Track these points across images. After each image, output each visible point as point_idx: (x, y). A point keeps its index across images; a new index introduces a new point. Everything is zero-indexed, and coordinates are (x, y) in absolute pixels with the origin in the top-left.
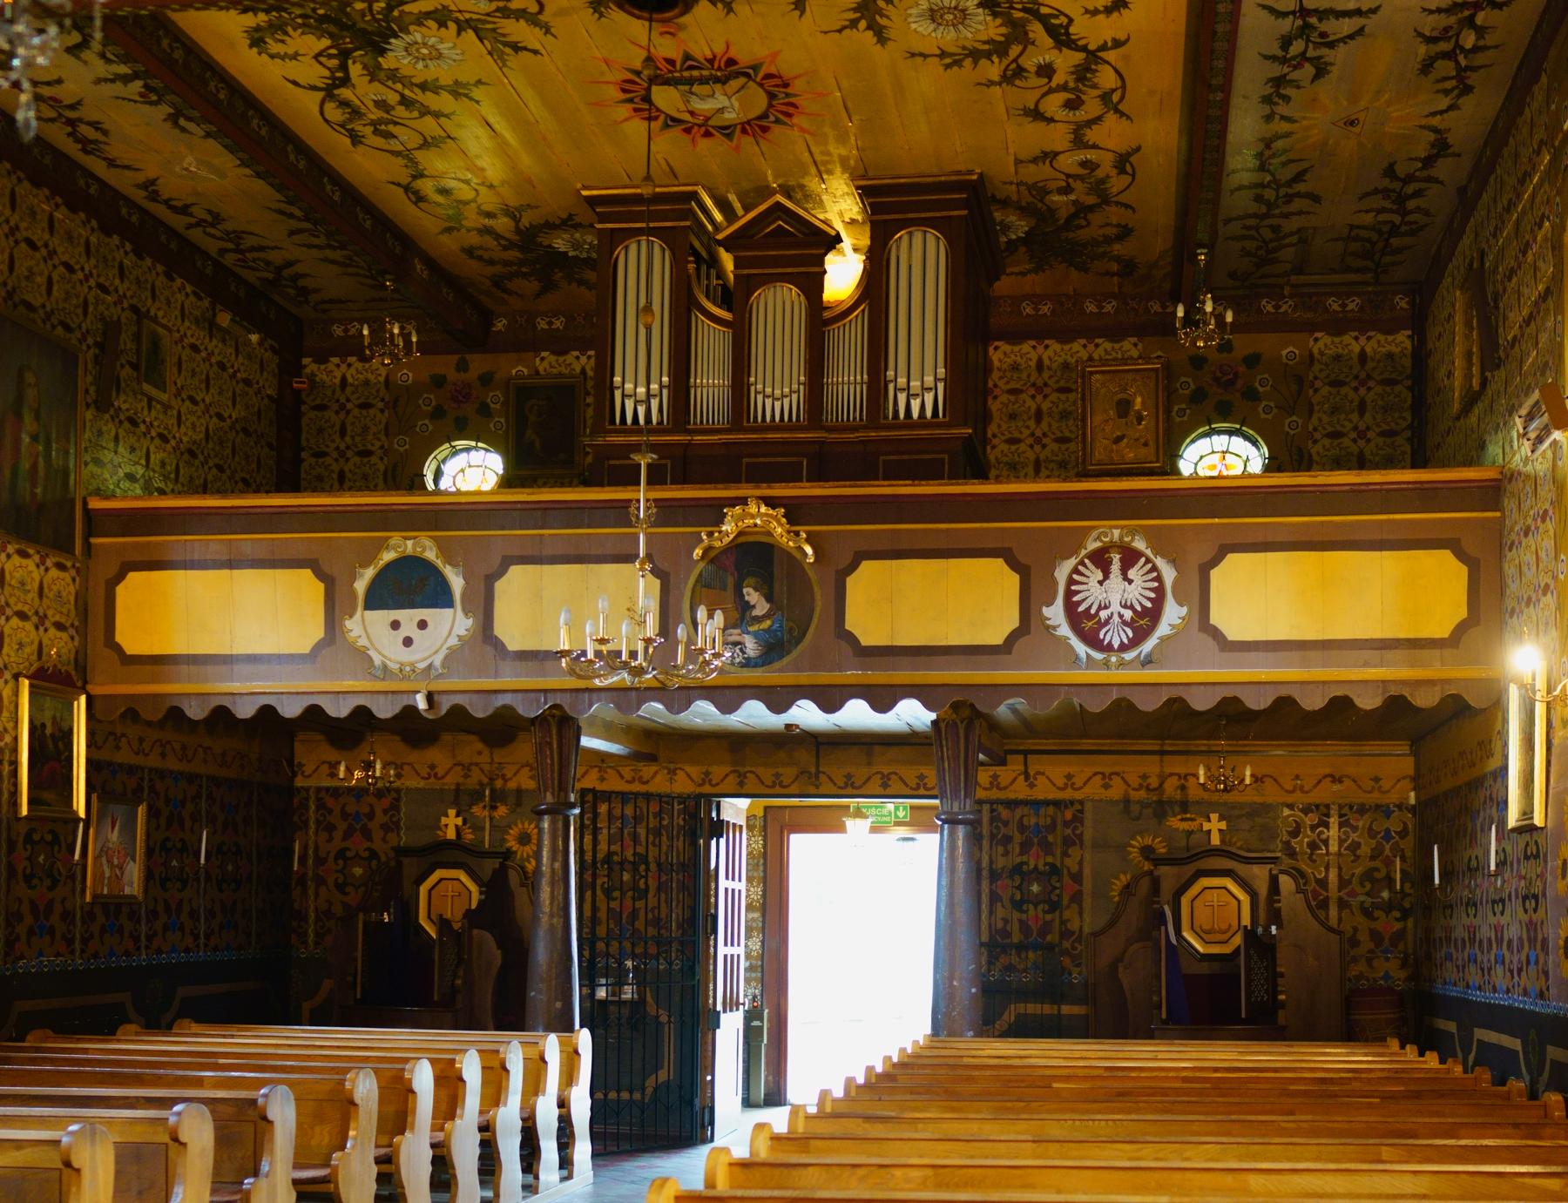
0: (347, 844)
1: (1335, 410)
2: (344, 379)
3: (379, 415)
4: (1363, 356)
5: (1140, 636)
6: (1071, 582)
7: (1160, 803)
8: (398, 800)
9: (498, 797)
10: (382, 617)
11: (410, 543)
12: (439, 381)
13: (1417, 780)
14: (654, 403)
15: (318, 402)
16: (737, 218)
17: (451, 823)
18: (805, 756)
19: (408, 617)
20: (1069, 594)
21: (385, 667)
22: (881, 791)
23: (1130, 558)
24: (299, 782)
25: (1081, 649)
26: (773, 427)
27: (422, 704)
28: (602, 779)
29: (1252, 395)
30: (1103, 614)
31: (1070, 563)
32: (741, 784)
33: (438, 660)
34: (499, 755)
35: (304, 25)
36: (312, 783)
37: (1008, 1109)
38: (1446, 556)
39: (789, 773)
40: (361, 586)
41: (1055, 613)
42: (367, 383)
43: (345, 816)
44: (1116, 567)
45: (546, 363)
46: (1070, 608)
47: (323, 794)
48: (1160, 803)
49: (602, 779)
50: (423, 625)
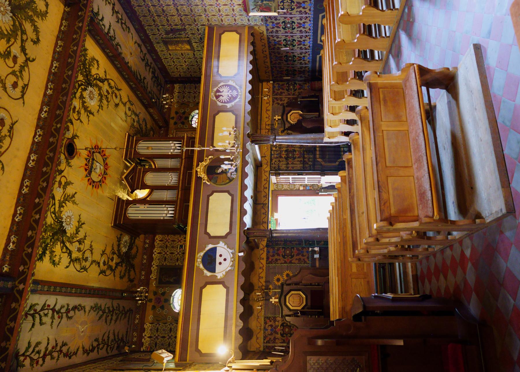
0: (285, 89)
1: (189, 97)
2: (149, 337)
3: (161, 326)
4: (178, 93)
5: (235, 89)
6: (222, 102)
7: (271, 129)
8: (267, 317)
9: (267, 288)
10: (218, 268)
11: (198, 260)
12: (154, 307)
13: (268, 81)
14: (169, 209)
15: (154, 345)
16: (129, 167)
17: (273, 300)
18: (259, 207)
19: (218, 259)
20: (225, 103)
21: (231, 266)
22: (268, 189)
23: (218, 91)
24: (262, 349)
25: (237, 100)
26: (179, 180)
27: (242, 254)
28: (263, 259)
29: (184, 113)
30: (230, 96)
31: (218, 103)
32: (265, 222)
33: (231, 251)
34: (256, 287)
35: (53, 243)
36: (262, 345)
37: (338, 270)
38: (223, 36)
39: (263, 211)
40: (209, 274)
41: (229, 105)
42: (151, 330)
43: (271, 334)
44: (220, 94)
45: (153, 276)
46: (228, 102)
47: (265, 341)
48: (271, 129)
49: (263, 259)
50: (221, 256)
